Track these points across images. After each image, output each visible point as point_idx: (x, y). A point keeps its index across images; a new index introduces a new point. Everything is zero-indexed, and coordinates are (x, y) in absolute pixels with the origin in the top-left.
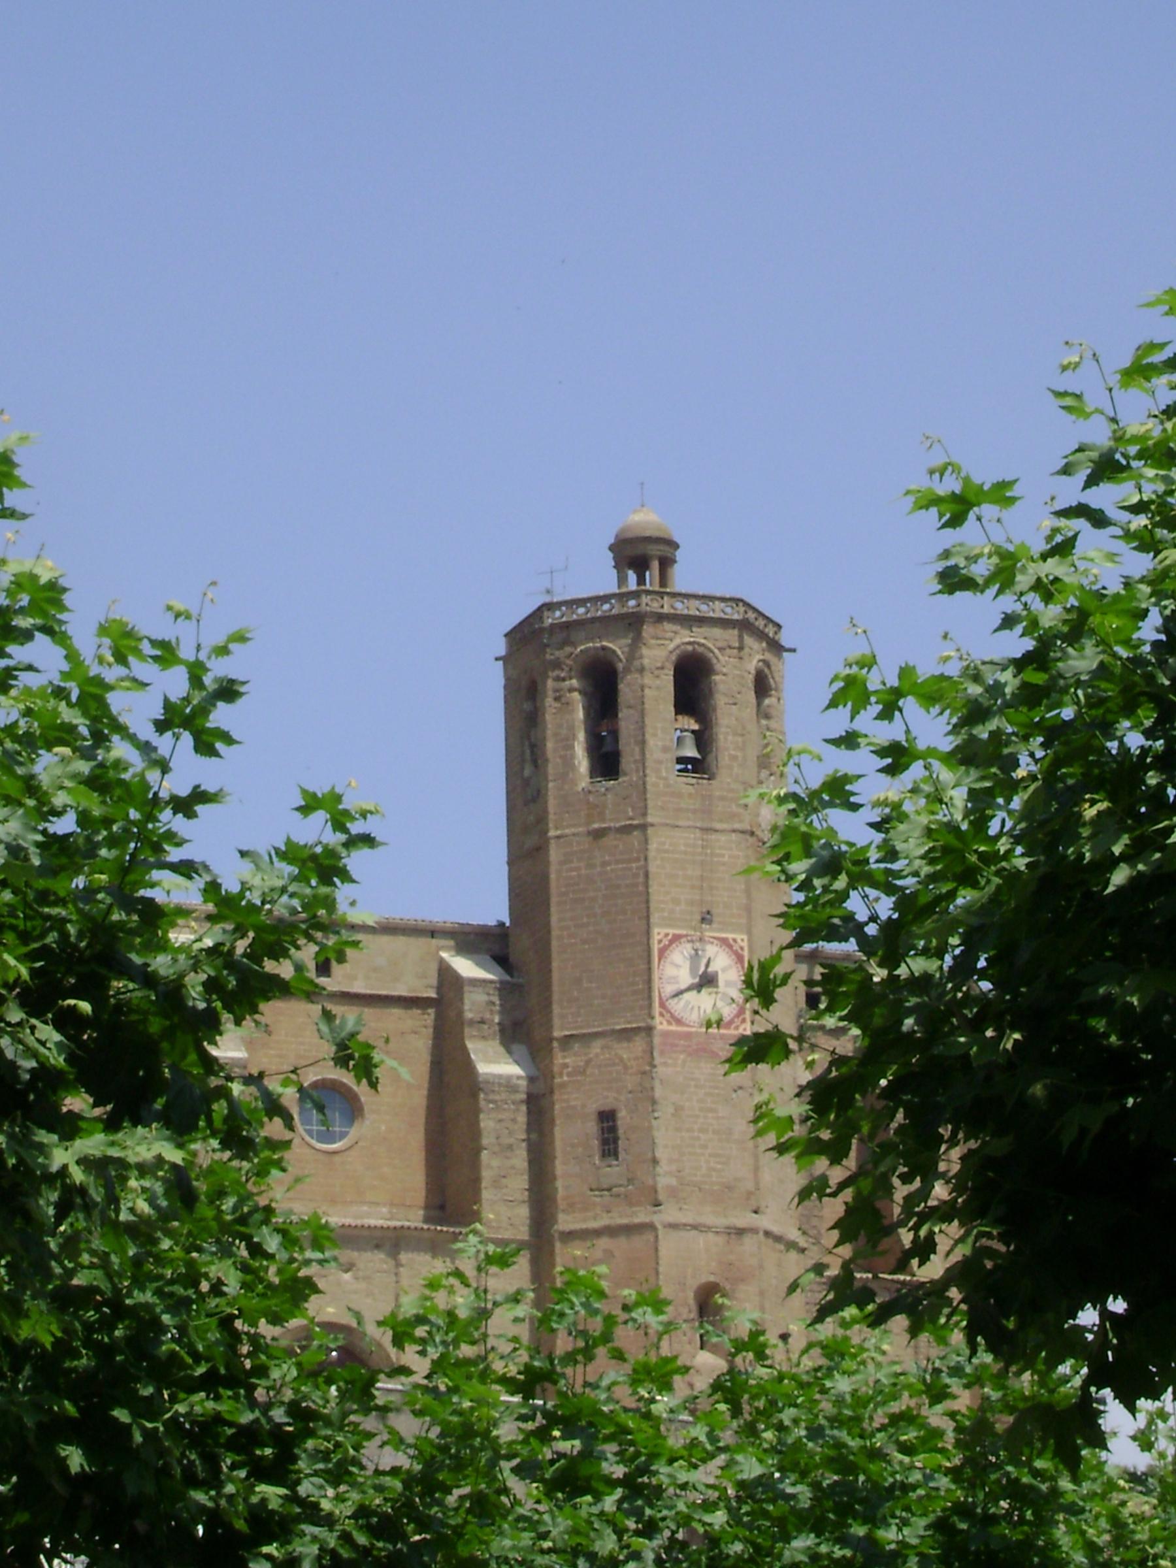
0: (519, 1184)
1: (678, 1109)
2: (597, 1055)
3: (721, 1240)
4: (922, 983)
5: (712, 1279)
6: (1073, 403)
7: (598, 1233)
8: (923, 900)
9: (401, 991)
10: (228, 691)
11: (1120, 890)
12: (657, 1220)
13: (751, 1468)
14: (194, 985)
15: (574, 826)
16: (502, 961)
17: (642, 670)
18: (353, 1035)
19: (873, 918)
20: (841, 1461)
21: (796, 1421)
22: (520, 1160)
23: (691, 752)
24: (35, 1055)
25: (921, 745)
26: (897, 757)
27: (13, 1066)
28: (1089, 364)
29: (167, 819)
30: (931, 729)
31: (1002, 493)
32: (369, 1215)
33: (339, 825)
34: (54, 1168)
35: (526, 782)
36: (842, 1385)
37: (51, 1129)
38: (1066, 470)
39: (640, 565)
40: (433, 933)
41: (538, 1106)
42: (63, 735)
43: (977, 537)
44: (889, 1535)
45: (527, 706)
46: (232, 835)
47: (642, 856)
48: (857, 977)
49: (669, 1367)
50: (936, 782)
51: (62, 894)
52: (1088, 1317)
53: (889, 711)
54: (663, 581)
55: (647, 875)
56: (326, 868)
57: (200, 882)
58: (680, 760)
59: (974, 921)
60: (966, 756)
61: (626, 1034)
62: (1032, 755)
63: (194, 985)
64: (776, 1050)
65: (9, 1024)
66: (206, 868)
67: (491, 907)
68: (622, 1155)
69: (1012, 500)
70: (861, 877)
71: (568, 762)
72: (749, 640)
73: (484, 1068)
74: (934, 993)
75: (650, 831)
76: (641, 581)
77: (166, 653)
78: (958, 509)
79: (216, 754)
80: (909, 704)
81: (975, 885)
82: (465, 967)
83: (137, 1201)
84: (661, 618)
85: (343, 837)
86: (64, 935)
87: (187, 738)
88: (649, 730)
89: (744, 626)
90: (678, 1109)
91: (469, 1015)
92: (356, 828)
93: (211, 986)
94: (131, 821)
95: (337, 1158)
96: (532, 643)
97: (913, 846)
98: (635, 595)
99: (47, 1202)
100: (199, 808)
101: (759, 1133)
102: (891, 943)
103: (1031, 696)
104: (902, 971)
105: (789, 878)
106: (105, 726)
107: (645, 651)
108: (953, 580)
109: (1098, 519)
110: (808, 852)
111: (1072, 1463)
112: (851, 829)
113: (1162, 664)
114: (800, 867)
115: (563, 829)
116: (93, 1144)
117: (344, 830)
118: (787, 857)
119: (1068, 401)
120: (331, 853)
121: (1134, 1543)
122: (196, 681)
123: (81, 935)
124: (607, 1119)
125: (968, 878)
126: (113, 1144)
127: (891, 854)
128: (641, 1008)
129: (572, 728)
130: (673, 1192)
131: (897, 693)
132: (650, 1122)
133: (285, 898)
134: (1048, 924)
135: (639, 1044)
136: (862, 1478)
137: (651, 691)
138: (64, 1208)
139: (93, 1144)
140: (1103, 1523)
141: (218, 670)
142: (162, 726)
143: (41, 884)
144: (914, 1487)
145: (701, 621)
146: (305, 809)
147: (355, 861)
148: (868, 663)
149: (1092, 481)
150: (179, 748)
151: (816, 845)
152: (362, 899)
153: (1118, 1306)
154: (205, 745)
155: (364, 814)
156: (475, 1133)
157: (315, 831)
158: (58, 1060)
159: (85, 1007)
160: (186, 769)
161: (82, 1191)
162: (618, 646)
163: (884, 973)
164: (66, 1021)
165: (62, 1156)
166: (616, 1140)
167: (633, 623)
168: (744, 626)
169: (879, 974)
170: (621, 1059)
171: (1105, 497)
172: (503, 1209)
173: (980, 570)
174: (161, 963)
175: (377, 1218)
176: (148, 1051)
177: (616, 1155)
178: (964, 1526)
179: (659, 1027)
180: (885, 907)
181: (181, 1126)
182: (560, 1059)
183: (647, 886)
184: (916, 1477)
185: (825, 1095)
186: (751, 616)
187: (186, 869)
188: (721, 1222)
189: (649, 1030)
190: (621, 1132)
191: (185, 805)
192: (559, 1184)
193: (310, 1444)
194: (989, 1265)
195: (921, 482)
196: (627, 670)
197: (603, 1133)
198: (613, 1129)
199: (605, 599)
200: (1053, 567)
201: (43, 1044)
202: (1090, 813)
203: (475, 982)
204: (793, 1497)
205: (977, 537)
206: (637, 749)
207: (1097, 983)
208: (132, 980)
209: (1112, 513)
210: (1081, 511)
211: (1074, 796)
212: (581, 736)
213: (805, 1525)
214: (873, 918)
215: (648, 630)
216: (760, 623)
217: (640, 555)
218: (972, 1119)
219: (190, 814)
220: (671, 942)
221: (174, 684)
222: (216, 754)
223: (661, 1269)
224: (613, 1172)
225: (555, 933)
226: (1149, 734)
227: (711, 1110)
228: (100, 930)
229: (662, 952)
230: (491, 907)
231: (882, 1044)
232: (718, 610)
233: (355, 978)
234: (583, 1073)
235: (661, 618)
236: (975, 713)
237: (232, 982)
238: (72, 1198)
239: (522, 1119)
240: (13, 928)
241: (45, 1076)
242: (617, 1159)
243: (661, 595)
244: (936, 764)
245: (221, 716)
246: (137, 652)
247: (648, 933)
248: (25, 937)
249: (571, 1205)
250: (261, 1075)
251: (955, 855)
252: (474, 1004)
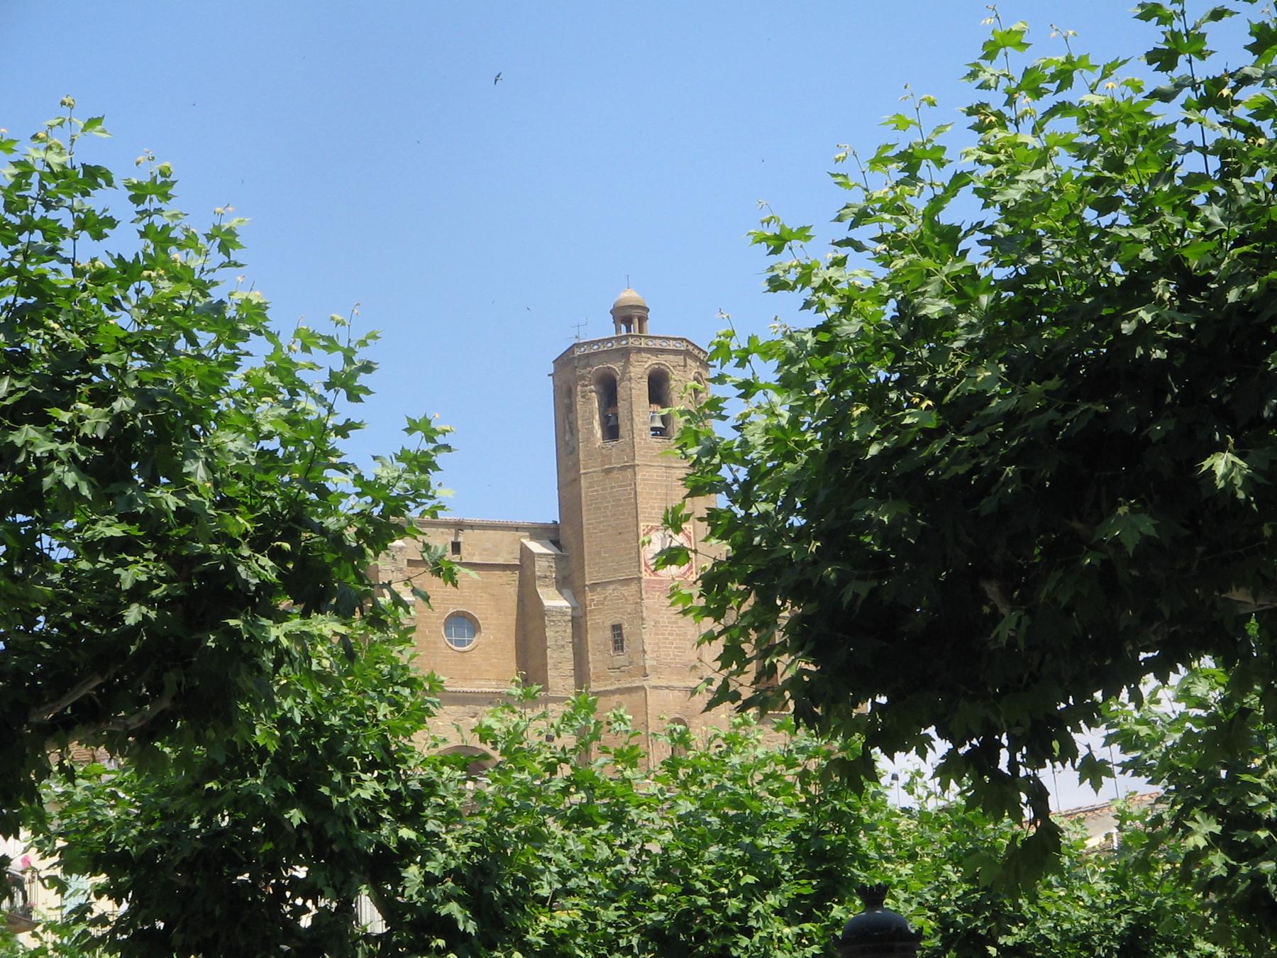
0: (569, 666)
1: (657, 622)
3: (682, 694)
4: (764, 517)
6: (842, 180)
7: (613, 692)
8: (763, 470)
9: (500, 561)
10: (368, 368)
11: (873, 457)
12: (645, 684)
13: (686, 806)
14: (350, 533)
16: (556, 543)
17: (630, 379)
18: (441, 557)
19: (736, 480)
20: (736, 802)
21: (710, 781)
22: (569, 652)
23: (659, 424)
24: (258, 575)
25: (761, 382)
26: (747, 389)
27: (247, 582)
28: (850, 157)
29: (334, 440)
30: (766, 371)
31: (803, 233)
32: (485, 686)
33: (430, 439)
34: (271, 640)
35: (567, 443)
36: (735, 760)
37: (269, 618)
38: (839, 219)
39: (628, 321)
40: (517, 529)
41: (578, 623)
42: (270, 391)
43: (787, 261)
44: (764, 842)
45: (566, 401)
46: (370, 449)
48: (728, 515)
49: (635, 753)
50: (770, 402)
51: (272, 483)
52: (867, 707)
53: (742, 362)
54: (641, 331)
56: (423, 464)
57: (351, 475)
58: (653, 429)
59: (793, 480)
60: (786, 384)
61: (626, 582)
62: (823, 382)
63: (350, 533)
64: (682, 558)
65: (243, 557)
66: (355, 467)
67: (550, 513)
69: (809, 237)
70: (728, 456)
71: (591, 432)
72: (689, 361)
73: (547, 603)
74: (771, 523)
76: (628, 330)
77: (330, 344)
78: (778, 243)
79: (361, 401)
80: (755, 358)
81: (794, 461)
82: (536, 547)
83: (324, 661)
84: (640, 350)
85: (432, 446)
86: (273, 508)
87: (343, 392)
88: (635, 414)
89: (687, 353)
90: (657, 622)
91: (538, 574)
92: (440, 440)
93: (360, 533)
94: (315, 447)
95: (466, 655)
96: (568, 366)
97: (757, 439)
98: (626, 337)
99: (268, 658)
100: (350, 432)
101: (672, 604)
102: (745, 495)
103: (824, 349)
104: (754, 511)
105: (686, 457)
106: (295, 387)
107: (632, 369)
108: (776, 284)
109: (859, 247)
110: (698, 442)
111: (859, 790)
112: (723, 431)
113: (896, 327)
114: (693, 451)
115: (589, 468)
116: (294, 624)
117: (434, 441)
118: (685, 445)
119: (839, 179)
120: (425, 454)
121: (906, 846)
122: (349, 360)
123: (283, 508)
124: (617, 628)
125: (790, 456)
126: (304, 624)
127: (745, 443)
129: (592, 412)
130: (654, 669)
131: (747, 352)
133: (400, 484)
134: (837, 480)
135: (634, 587)
136: (748, 811)
137: (636, 390)
138: (278, 664)
139: (294, 624)
140: (887, 835)
141: (360, 356)
142: (328, 386)
143: (259, 477)
144: (778, 816)
145: (663, 351)
146: (410, 430)
147: (440, 459)
148: (731, 335)
149: (854, 225)
150: (339, 398)
151: (702, 438)
152: (451, 490)
153: (883, 700)
154: (353, 397)
155: (444, 433)
156: (544, 639)
157: (416, 443)
158: (272, 577)
159: (287, 546)
160: (345, 410)
161: (288, 652)
162: (617, 367)
163: (742, 513)
164: (277, 555)
165: (275, 632)
166: (622, 641)
167: (625, 353)
168: (687, 353)
169: (741, 513)
171: (865, 233)
172: (560, 678)
173: (791, 278)
174: (331, 523)
175: (489, 687)
176: (325, 572)
178: (807, 837)
180: (742, 474)
181: (344, 614)
182: (589, 596)
184: (778, 810)
185: (713, 582)
186: (690, 348)
187: (343, 468)
188: (682, 684)
189: (640, 579)
191: (343, 431)
192: (591, 666)
193: (432, 799)
194: (806, 678)
195: (756, 229)
196: (622, 380)
198: (620, 635)
199: (609, 340)
200: (834, 273)
201: (263, 568)
202: (856, 413)
203: (540, 555)
204: (710, 823)
205: (787, 261)
207: (863, 510)
208: (312, 531)
209: (867, 243)
210: (848, 242)
211: (849, 403)
212: (597, 417)
214: (736, 480)
215: (633, 357)
216: (696, 352)
217: (628, 316)
218: (796, 594)
219: (345, 436)
221: (336, 362)
222: (361, 401)
224: (621, 659)
225: (585, 527)
226: (890, 370)
227: (675, 623)
228: (295, 504)
230: (550, 513)
231: (743, 551)
232: (672, 345)
235: (640, 350)
236: (790, 359)
237: (371, 529)
238: (282, 657)
239: (569, 630)
240: (245, 504)
241: (264, 585)
243: (640, 337)
244: (770, 392)
245: (363, 379)
246: (316, 344)
248: (252, 509)
249: (598, 677)
250: (390, 583)
251: (781, 444)
252: (541, 567)
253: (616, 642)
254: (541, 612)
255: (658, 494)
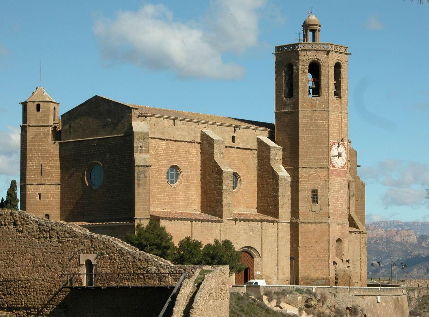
2: (312, 174)
5: (339, 237)
12: (329, 221)
15: (307, 108)
32: (242, 211)
47: (327, 119)
55: (329, 125)
68: (151, 151)
75: (330, 112)
124: (315, 193)
128: (326, 162)
132: (327, 194)
166: (317, 198)
170: (320, 176)
177: (317, 202)
179: (330, 168)
183: (328, 128)
190: (319, 196)
197: (313, 196)
198: (317, 195)
206: (326, 89)
213: (191, 307)
217: (308, 28)
220: (333, 144)
223: (330, 235)
229: (331, 147)
233: (240, 143)
234: (308, 178)
242: (318, 203)
247: (329, 142)
253: (313, 198)
254: (275, 177)
255: (336, 126)
